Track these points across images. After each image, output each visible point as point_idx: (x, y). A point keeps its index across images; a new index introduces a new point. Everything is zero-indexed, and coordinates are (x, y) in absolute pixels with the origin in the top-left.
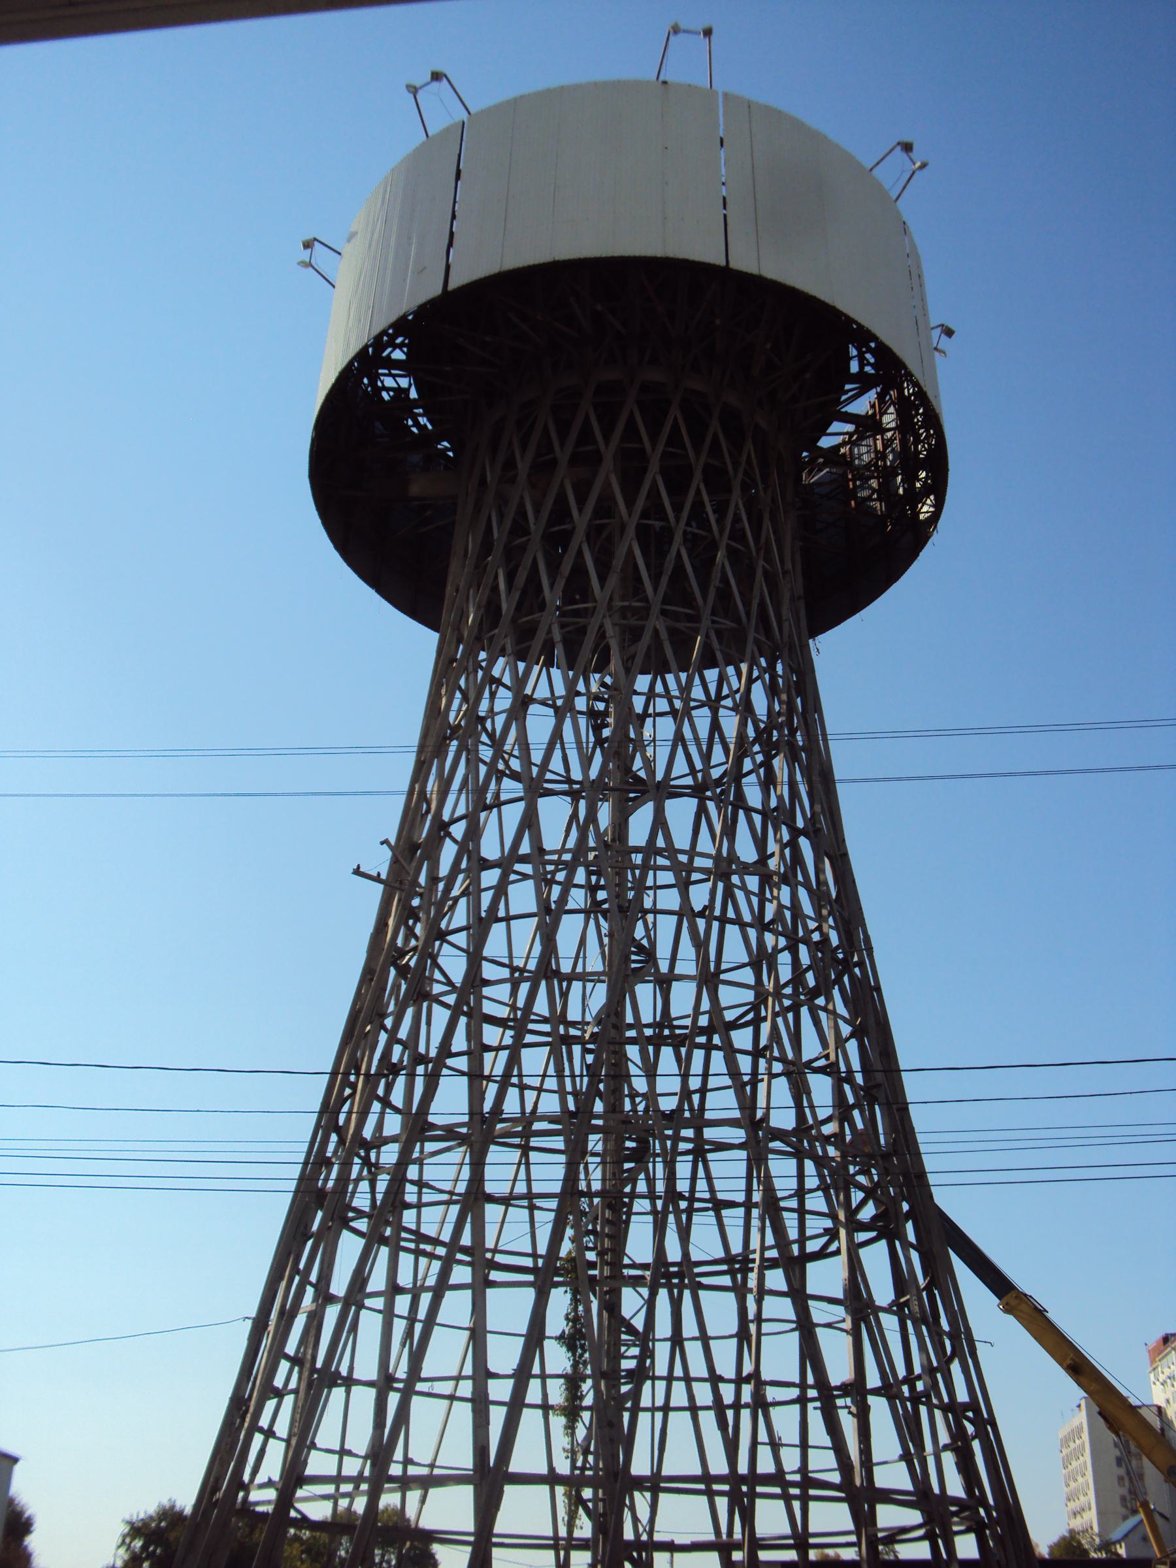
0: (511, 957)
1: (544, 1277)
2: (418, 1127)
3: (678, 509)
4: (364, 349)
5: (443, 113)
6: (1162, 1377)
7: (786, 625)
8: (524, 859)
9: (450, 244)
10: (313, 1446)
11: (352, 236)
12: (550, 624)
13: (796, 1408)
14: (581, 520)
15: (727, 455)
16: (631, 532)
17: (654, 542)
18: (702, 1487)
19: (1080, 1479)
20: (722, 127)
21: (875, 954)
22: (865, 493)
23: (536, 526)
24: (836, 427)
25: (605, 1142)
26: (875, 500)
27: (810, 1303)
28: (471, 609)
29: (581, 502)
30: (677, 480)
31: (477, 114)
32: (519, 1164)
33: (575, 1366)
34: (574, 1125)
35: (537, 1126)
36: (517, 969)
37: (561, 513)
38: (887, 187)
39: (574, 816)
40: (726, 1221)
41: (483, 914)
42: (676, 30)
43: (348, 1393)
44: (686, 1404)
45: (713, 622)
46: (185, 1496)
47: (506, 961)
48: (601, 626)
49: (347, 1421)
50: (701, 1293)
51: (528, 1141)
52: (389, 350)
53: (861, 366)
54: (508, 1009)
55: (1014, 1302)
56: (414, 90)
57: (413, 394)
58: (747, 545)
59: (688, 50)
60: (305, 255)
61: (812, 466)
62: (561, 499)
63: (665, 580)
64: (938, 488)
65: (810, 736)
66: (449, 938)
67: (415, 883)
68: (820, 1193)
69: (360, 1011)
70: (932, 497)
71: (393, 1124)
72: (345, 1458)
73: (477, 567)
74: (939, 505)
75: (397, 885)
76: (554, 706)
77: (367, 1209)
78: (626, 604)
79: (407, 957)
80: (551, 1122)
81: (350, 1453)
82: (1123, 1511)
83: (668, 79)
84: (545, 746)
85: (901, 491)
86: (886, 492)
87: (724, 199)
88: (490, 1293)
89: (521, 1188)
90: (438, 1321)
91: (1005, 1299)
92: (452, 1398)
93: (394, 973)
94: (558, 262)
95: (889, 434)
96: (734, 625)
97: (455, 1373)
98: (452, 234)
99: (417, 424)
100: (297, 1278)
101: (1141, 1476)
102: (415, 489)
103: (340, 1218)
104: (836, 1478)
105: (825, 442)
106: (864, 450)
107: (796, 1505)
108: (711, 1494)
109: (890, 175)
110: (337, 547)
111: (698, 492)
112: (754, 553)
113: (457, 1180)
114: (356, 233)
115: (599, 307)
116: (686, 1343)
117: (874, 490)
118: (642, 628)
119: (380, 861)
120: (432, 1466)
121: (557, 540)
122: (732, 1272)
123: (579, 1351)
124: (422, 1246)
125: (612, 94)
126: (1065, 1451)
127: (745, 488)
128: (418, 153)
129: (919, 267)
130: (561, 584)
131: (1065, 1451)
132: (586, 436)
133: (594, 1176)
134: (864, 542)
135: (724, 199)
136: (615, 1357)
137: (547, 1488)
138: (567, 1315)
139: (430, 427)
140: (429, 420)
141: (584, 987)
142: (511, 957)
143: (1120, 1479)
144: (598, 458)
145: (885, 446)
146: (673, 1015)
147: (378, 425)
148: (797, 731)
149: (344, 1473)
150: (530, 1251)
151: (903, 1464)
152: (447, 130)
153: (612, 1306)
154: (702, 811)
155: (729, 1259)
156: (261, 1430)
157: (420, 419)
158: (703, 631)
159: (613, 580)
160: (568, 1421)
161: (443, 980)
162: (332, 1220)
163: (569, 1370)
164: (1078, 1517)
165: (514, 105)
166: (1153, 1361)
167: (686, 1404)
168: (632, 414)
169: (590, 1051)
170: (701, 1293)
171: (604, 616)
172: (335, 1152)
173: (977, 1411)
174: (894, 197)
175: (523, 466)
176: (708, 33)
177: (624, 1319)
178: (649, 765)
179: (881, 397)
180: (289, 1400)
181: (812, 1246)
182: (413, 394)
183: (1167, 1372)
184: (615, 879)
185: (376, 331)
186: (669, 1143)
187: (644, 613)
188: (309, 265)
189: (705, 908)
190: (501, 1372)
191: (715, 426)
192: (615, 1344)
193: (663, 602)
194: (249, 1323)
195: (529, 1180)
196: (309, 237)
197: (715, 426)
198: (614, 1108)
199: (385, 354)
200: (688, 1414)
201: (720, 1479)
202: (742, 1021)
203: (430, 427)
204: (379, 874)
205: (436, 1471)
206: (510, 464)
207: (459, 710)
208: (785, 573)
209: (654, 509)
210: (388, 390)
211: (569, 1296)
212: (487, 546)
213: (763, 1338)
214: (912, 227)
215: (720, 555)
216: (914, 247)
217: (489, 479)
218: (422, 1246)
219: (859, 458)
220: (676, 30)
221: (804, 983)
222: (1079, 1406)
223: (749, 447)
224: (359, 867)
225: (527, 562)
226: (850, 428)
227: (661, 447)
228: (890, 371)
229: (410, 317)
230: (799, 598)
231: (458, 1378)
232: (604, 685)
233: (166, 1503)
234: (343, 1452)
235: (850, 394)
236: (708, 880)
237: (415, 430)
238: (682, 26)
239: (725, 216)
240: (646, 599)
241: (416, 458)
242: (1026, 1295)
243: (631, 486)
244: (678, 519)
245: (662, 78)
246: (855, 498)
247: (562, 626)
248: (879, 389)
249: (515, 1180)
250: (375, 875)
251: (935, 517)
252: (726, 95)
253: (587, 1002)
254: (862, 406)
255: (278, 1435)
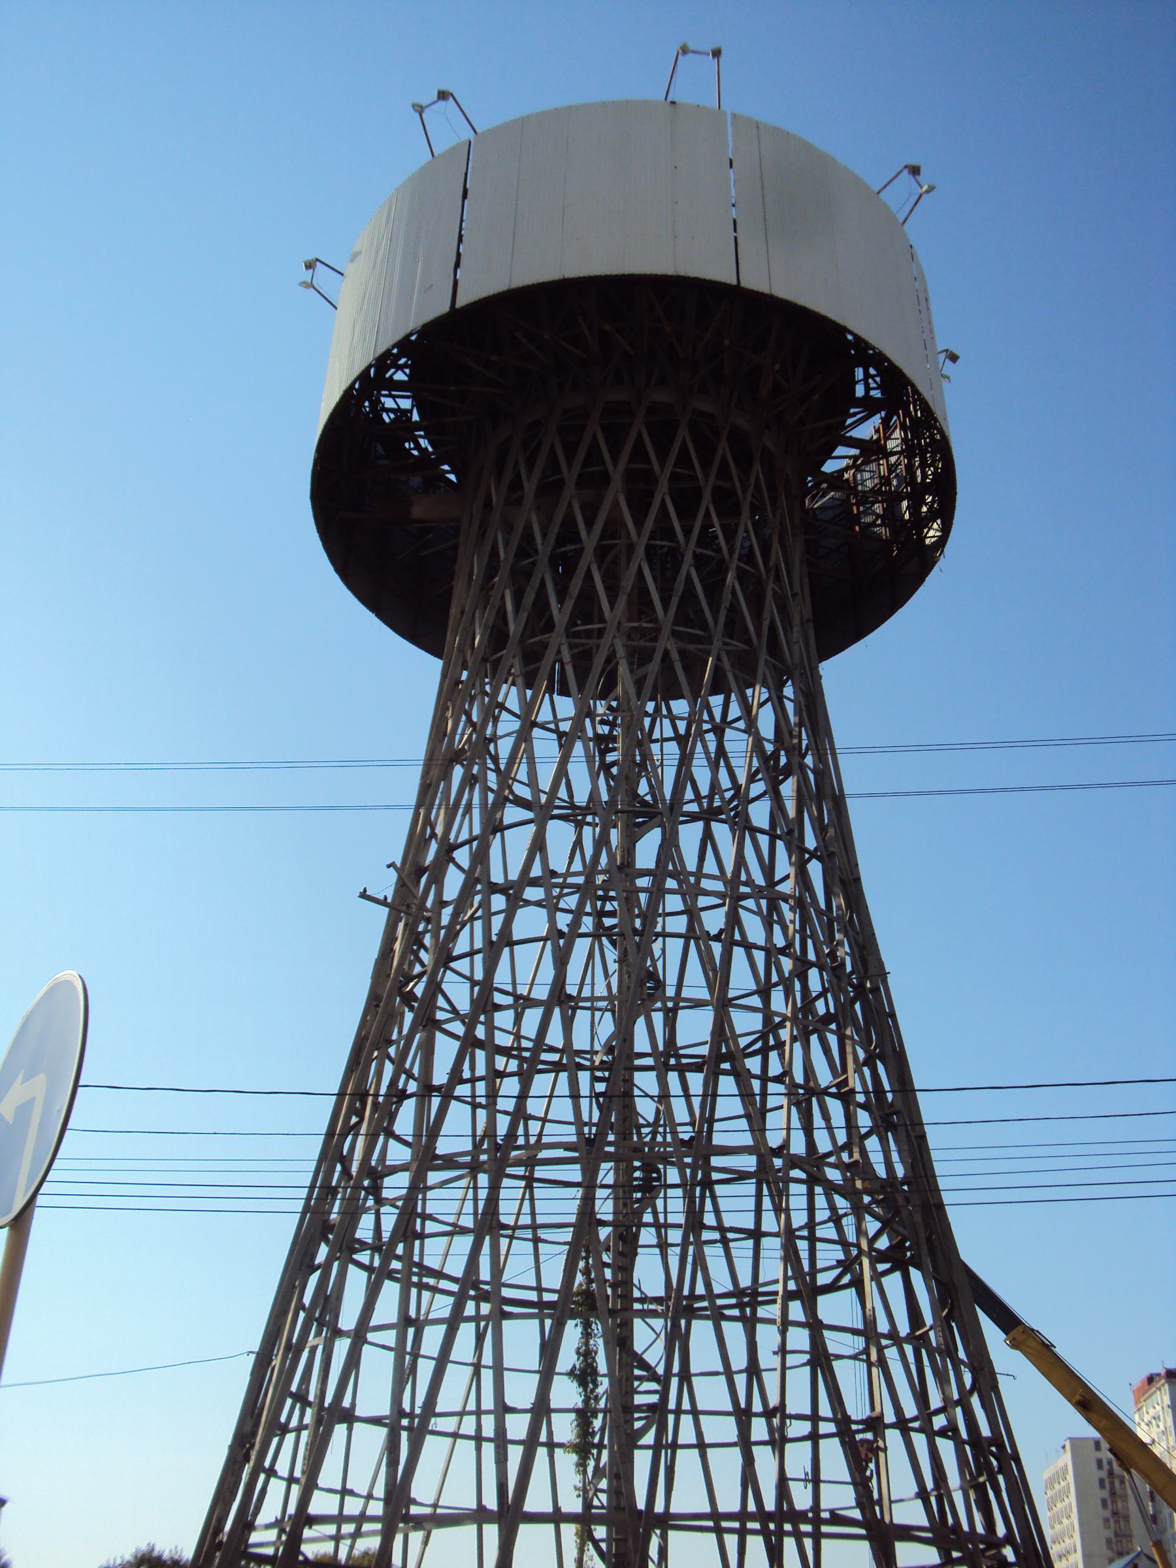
0: (514, 983)
1: (555, 1311)
2: (427, 1157)
3: (687, 531)
4: (366, 372)
5: (448, 131)
6: (1147, 1418)
7: (796, 648)
8: (534, 882)
9: (457, 265)
10: (316, 1487)
11: (354, 257)
12: (559, 645)
13: (808, 1444)
14: (589, 540)
15: (735, 478)
16: (640, 552)
17: (665, 562)
18: (710, 1524)
19: (1065, 1521)
20: (731, 147)
21: (673, 1493)
22: (869, 519)
23: (543, 547)
24: (841, 451)
25: (617, 1170)
26: (879, 526)
27: (826, 1333)
28: (478, 631)
29: (589, 524)
30: (687, 501)
31: (483, 134)
32: (523, 1199)
33: (586, 1401)
34: (588, 1151)
35: (544, 1154)
36: (520, 997)
37: (569, 533)
38: (894, 209)
39: (578, 843)
40: (734, 1252)
41: (494, 938)
42: (685, 50)
43: (350, 1430)
44: (694, 1441)
45: (725, 644)
46: (413, 1495)
47: (509, 988)
48: (612, 645)
49: (357, 1458)
50: (724, 1324)
51: (532, 1172)
52: (392, 371)
53: (868, 389)
54: (512, 1037)
55: (1021, 1337)
56: (420, 109)
57: (416, 417)
58: (756, 567)
59: (697, 69)
60: (307, 275)
61: (817, 493)
62: (569, 520)
63: (675, 601)
64: (945, 512)
65: (820, 757)
66: (452, 965)
67: (422, 907)
68: (831, 1224)
69: (366, 1038)
70: (939, 521)
71: (398, 1154)
72: (347, 1498)
73: (482, 588)
74: (946, 530)
75: (404, 908)
76: (556, 731)
77: (370, 1241)
78: (636, 624)
79: (411, 984)
80: (566, 1149)
81: (352, 1493)
82: (1110, 1554)
83: (676, 100)
84: (571, 759)
85: (907, 516)
86: (891, 516)
87: (735, 221)
88: (506, 1324)
89: (525, 1220)
90: (433, 1363)
91: (1013, 1333)
92: (455, 1435)
93: (395, 1003)
94: (569, 279)
95: (893, 459)
96: (746, 647)
97: (458, 1408)
98: (459, 255)
99: (417, 446)
100: (302, 1315)
101: (1127, 1518)
102: (417, 512)
103: (346, 1248)
104: (856, 1514)
105: (830, 467)
106: (867, 475)
107: (808, 1543)
108: (719, 1531)
109: (897, 197)
110: (337, 570)
111: (707, 514)
112: (764, 575)
113: (460, 1214)
114: (360, 253)
115: (607, 327)
116: (693, 1378)
117: (878, 516)
118: (653, 650)
119: (386, 884)
120: (435, 1506)
121: (565, 563)
122: (740, 1306)
123: (591, 1386)
124: (425, 1280)
125: (621, 115)
126: (1050, 1493)
127: (754, 509)
128: (423, 174)
129: (926, 291)
130: (569, 604)
131: (1050, 1493)
132: (593, 456)
133: (605, 1208)
134: (872, 568)
135: (735, 221)
136: (627, 1393)
137: (551, 1527)
138: (578, 1349)
139: (430, 449)
140: (430, 443)
141: (593, 1016)
142: (514, 983)
143: (1106, 1520)
144: (606, 479)
145: (890, 472)
146: (679, 1044)
147: (379, 448)
148: (804, 752)
149: (346, 1512)
150: (534, 1284)
151: (919, 1502)
152: (453, 150)
153: (621, 1342)
154: (708, 836)
155: (738, 1292)
156: (264, 1470)
157: (421, 441)
158: (714, 652)
159: (622, 601)
160: (580, 1458)
161: (448, 1008)
162: (340, 1250)
163: (580, 1405)
164: (1064, 1560)
165: (522, 123)
166: (1137, 1401)
167: (694, 1441)
168: (640, 436)
169: (600, 1080)
170: (724, 1324)
171: (614, 637)
172: (339, 1181)
173: (1000, 1446)
174: (901, 220)
175: (530, 488)
176: (717, 53)
177: (636, 1353)
178: (656, 787)
179: (885, 422)
180: (305, 1434)
181: (823, 1279)
182: (416, 417)
183: (1152, 1412)
184: (620, 909)
185: (381, 349)
186: (688, 1171)
187: (654, 635)
188: (310, 285)
189: (721, 931)
190: (519, 1407)
191: (723, 447)
192: (627, 1379)
193: (674, 624)
194: (253, 1356)
195: (533, 1214)
196: (311, 257)
197: (723, 447)
198: (624, 1136)
199: (387, 375)
200: (696, 1451)
201: (729, 1516)
202: (751, 1050)
203: (430, 449)
204: (386, 898)
205: (439, 1511)
206: (516, 485)
207: (463, 734)
208: (795, 595)
209: (664, 530)
210: (388, 410)
211: (580, 1329)
212: (492, 570)
213: (788, 1372)
214: (919, 251)
215: (730, 577)
216: (920, 270)
217: (494, 499)
218: (425, 1280)
219: (862, 484)
220: (685, 50)
221: (814, 1012)
222: (1064, 1447)
223: (757, 468)
224: (365, 890)
225: (535, 582)
226: (854, 452)
227: (669, 468)
228: (898, 393)
229: (413, 338)
230: (808, 621)
231: (462, 1414)
232: (610, 708)
233: (144, 1547)
234: (345, 1492)
235: (859, 416)
236: (723, 905)
237: (415, 453)
238: (692, 46)
239: (736, 238)
240: (655, 620)
241: (416, 481)
242: (1033, 1330)
243: (640, 510)
244: (687, 542)
245: (670, 98)
246: (859, 524)
247: (571, 647)
248: (883, 413)
249: (518, 1214)
250: (382, 898)
251: (942, 542)
252: (734, 116)
253: (592, 1031)
254: (866, 431)
255: (280, 1474)
